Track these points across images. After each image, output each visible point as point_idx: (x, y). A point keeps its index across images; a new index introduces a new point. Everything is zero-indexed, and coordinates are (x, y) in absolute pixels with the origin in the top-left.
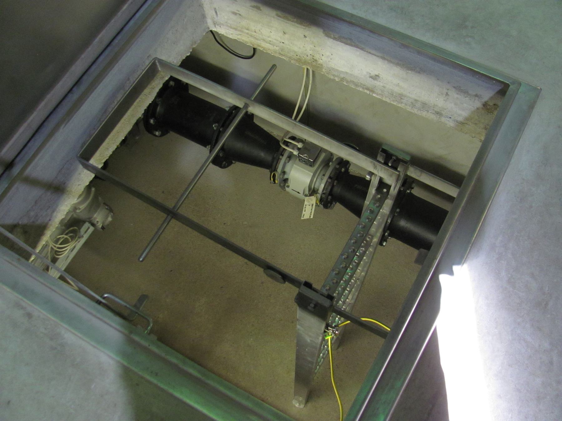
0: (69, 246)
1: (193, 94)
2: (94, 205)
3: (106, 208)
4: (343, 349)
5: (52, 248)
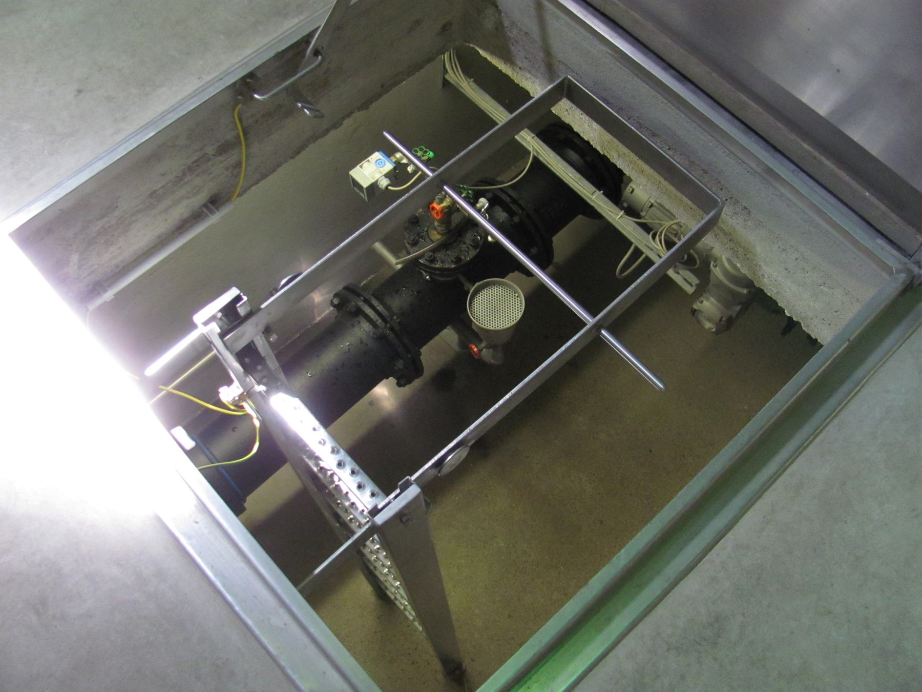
0: (662, 246)
1: (565, 229)
2: (728, 298)
3: (722, 317)
4: (440, 683)
5: (664, 224)
